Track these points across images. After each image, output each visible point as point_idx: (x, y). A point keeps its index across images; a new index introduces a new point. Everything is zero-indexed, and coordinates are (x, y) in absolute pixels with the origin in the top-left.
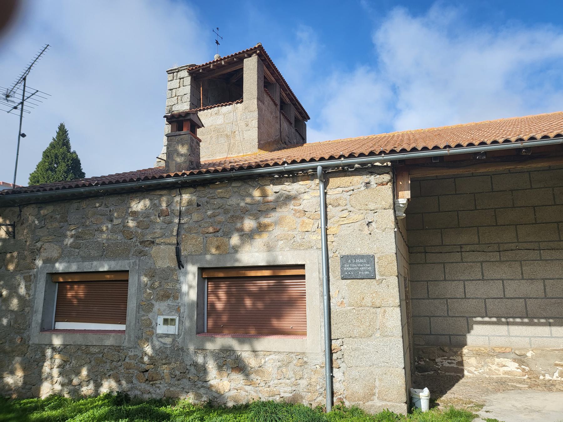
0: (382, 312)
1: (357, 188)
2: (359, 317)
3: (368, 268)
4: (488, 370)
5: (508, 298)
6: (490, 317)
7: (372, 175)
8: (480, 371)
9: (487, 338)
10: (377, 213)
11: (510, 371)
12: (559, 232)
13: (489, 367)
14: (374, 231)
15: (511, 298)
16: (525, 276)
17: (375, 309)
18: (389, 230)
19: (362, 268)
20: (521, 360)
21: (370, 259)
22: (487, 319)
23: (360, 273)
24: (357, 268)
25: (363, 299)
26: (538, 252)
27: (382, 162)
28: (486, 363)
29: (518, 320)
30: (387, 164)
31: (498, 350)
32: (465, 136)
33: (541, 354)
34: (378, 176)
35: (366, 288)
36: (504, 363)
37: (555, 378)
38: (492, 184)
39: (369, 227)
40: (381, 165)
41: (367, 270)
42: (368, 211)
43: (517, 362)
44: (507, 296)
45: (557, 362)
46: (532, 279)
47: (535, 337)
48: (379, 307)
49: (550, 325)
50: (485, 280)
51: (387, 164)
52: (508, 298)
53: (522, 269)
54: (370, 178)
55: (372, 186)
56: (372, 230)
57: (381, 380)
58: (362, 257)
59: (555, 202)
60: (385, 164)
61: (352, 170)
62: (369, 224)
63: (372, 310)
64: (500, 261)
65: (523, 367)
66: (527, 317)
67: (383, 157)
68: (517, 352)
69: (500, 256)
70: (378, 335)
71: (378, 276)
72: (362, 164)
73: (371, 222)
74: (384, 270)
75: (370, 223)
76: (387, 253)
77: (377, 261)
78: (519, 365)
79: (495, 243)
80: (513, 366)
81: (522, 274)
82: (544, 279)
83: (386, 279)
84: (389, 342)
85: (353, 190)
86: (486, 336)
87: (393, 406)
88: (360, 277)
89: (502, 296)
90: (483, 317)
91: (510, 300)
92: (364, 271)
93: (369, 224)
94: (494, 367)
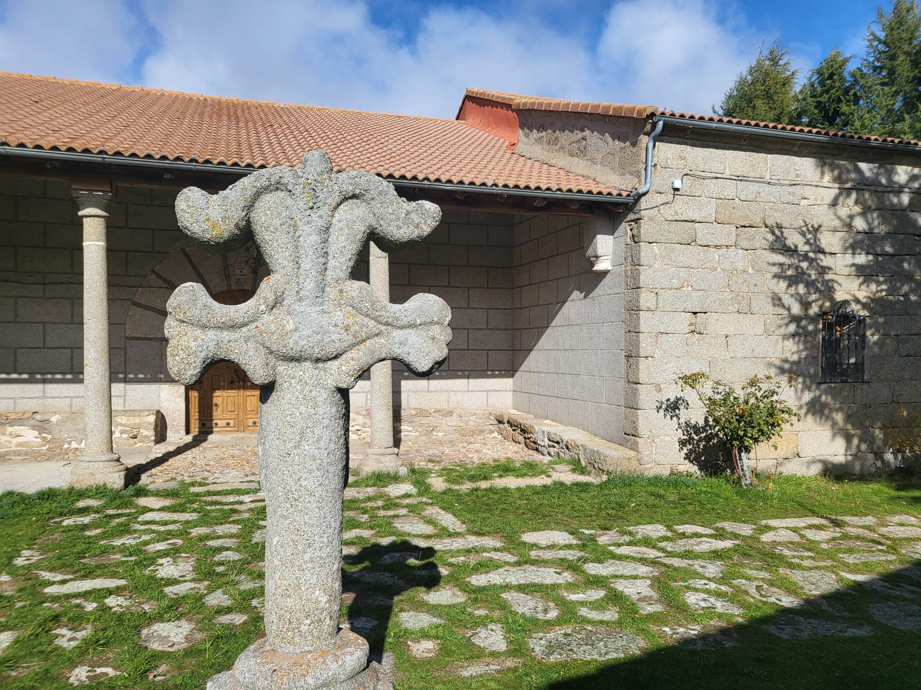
5: (49, 348)
6: (20, 374)
12: (126, 265)
15: (54, 348)
20: (42, 426)
22: (14, 376)
29: (59, 376)
32: (335, 156)
33: (68, 418)
36: (18, 433)
44: (48, 345)
50: (18, 322)
52: (49, 348)
65: (44, 435)
69: (44, 290)
78: (40, 434)
79: (39, 272)
81: (72, 316)
86: (12, 398)
89: (40, 346)
90: (8, 373)
91: (50, 350)
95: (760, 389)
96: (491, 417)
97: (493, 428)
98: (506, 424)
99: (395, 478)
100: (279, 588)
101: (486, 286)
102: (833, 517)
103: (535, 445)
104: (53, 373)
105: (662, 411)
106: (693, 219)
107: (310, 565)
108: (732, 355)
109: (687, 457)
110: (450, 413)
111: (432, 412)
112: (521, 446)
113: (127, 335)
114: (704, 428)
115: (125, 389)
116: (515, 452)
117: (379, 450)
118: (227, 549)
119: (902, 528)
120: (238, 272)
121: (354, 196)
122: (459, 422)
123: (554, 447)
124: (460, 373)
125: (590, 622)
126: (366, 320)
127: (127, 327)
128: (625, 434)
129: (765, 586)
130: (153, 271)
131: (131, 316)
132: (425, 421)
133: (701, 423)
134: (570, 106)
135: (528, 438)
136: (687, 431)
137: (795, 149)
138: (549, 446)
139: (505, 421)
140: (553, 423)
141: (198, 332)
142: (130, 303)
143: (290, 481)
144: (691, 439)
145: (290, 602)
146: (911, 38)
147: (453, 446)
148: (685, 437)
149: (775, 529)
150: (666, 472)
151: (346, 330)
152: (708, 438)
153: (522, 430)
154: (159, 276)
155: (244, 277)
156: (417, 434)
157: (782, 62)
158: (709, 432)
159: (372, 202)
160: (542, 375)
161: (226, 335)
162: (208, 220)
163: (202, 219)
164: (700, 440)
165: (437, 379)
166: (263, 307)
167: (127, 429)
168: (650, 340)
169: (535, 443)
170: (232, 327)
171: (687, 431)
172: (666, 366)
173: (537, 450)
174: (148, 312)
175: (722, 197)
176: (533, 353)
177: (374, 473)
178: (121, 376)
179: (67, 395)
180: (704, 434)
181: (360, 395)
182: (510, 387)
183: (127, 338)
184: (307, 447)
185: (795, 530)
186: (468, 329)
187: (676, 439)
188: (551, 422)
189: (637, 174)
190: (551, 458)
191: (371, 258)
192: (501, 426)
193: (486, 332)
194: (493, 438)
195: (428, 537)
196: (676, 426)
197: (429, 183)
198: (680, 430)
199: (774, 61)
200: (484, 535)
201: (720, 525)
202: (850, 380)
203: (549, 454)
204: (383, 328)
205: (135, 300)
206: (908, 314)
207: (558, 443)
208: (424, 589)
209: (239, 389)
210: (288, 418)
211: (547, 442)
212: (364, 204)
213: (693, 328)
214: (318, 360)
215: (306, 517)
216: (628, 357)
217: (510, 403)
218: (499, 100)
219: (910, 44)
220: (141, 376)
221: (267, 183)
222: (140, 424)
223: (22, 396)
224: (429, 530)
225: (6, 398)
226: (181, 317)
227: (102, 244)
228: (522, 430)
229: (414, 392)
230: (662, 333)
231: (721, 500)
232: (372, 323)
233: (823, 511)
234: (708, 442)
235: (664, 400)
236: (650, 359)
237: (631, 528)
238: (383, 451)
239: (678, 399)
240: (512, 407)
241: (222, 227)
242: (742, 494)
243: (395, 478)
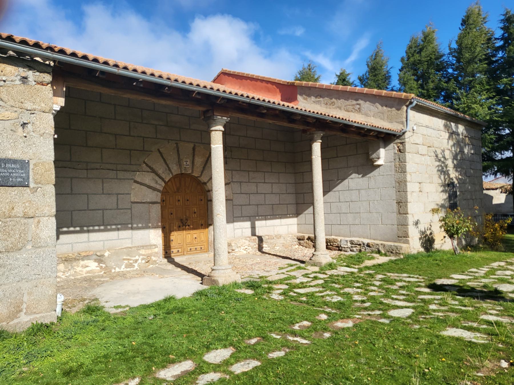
0: (36, 222)
1: (10, 80)
2: (7, 230)
3: (22, 175)
4: (74, 273)
5: (90, 210)
6: (75, 227)
7: (30, 70)
8: (67, 275)
9: (71, 245)
10: (35, 115)
11: (91, 270)
13: (75, 270)
14: (31, 134)
16: (105, 192)
17: (27, 219)
18: (48, 136)
19: (14, 174)
20: (100, 259)
21: (24, 165)
22: (72, 229)
23: (11, 179)
24: (7, 174)
25: (13, 209)
26: (115, 172)
27: (45, 58)
28: (72, 267)
29: (96, 228)
30: (50, 63)
31: (83, 254)
34: (38, 74)
35: (17, 197)
36: (87, 265)
37: (122, 270)
38: (85, 108)
39: (25, 129)
40: (42, 61)
41: (21, 177)
42: (23, 110)
43: (97, 262)
44: (90, 208)
45: (125, 257)
46: (109, 194)
47: (107, 240)
48: (32, 218)
49: (118, 229)
50: (74, 194)
51: (50, 63)
53: (103, 186)
54: (28, 73)
55: (30, 83)
56: (28, 133)
57: (30, 294)
58: (15, 161)
59: (156, 136)
60: (47, 62)
61: (4, 56)
62: (24, 125)
63: (23, 221)
64: (88, 178)
65: (101, 265)
66: (103, 225)
67: (48, 54)
68: (98, 254)
69: (87, 174)
70: (29, 247)
71: (32, 184)
72: (20, 53)
73: (27, 124)
74: (41, 178)
75: (25, 124)
76: (44, 160)
77: (32, 168)
78: (99, 264)
80: (93, 265)
81: (103, 189)
82: (118, 194)
83: (41, 188)
84: (42, 253)
85: (4, 81)
86: (70, 243)
87: (43, 317)
88: (11, 184)
90: (68, 227)
91: (91, 211)
92: (16, 177)
93: (24, 125)
94: (78, 269)
101: (270, 171)
104: (93, 226)
113: (132, 201)
115: (132, 234)
120: (185, 163)
124: (278, 216)
127: (132, 196)
128: (398, 237)
130: (144, 162)
131: (134, 189)
132: (272, 241)
137: (439, 116)
142: (133, 181)
154: (147, 165)
155: (188, 166)
156: (269, 248)
167: (145, 257)
174: (142, 187)
178: (130, 226)
179: (101, 239)
182: (296, 223)
183: (133, 203)
189: (402, 123)
205: (136, 179)
209: (183, 230)
211: (349, 245)
216: (398, 203)
220: (140, 225)
222: (151, 253)
223: (76, 242)
225: (67, 244)
227: (213, 146)
229: (261, 227)
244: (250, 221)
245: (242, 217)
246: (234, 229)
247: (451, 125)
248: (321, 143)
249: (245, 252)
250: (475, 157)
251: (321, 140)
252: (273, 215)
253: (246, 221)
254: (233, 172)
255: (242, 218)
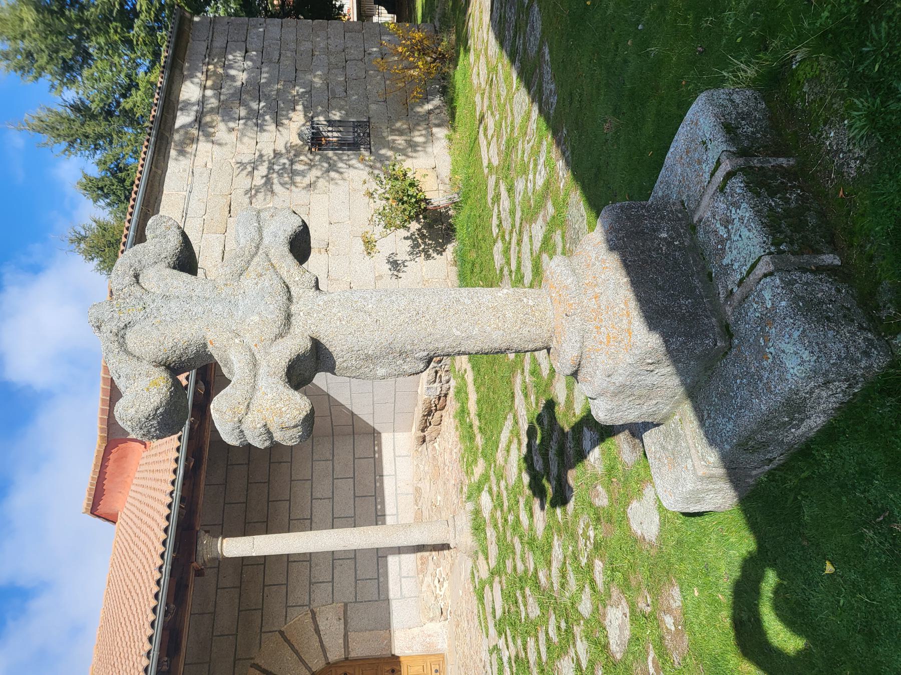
95: (376, 190)
96: (420, 450)
97: (430, 448)
98: (426, 433)
99: (477, 512)
100: (498, 325)
101: (289, 464)
102: (478, 122)
103: (442, 398)
105: (400, 275)
106: (221, 252)
107: (475, 299)
108: (347, 219)
109: (440, 253)
110: (418, 490)
111: (417, 508)
112: (444, 414)
114: (414, 241)
116: (448, 419)
117: (450, 533)
118: (547, 633)
119: (481, 73)
121: (137, 276)
122: (426, 481)
123: (440, 376)
124: (378, 484)
125: (564, 246)
126: (253, 263)
129: (527, 138)
133: (409, 242)
134: (106, 387)
135: (436, 406)
136: (417, 254)
137: (160, 172)
138: (441, 382)
139: (422, 434)
140: (420, 384)
141: (259, 394)
143: (402, 318)
144: (423, 250)
145: (509, 315)
146: (68, 120)
147: (448, 480)
148: (423, 254)
149: (489, 160)
150: (455, 269)
151: (261, 276)
152: (423, 236)
153: (429, 415)
157: (83, 233)
158: (417, 236)
159: (143, 263)
160: (375, 399)
161: (262, 371)
162: (148, 389)
163: (146, 394)
164: (424, 243)
165: (384, 507)
166: (237, 341)
168: (334, 286)
169: (439, 398)
170: (255, 365)
171: (417, 254)
172: (359, 272)
173: (446, 395)
175: (201, 229)
176: (356, 412)
177: (474, 535)
180: (419, 240)
181: (404, 584)
182: (391, 434)
184: (370, 306)
185: (489, 144)
186: (333, 479)
187: (424, 262)
188: (420, 388)
190: (452, 379)
191: (254, 555)
192: (427, 439)
193: (336, 462)
194: (439, 446)
195: (520, 443)
196: (413, 262)
197: (175, 492)
198: (416, 260)
199: (81, 239)
200: (513, 393)
201: (490, 201)
202: (368, 131)
203: (448, 382)
204: (261, 251)
206: (311, 91)
207: (436, 372)
208: (556, 408)
210: (344, 323)
211: (437, 385)
212: (144, 271)
213: (323, 251)
214: (290, 299)
215: (433, 304)
217: (406, 434)
218: (98, 470)
219: (74, 121)
221: (116, 343)
224: (514, 446)
226: (243, 407)
228: (429, 415)
230: (328, 276)
231: (472, 214)
232: (256, 259)
233: (474, 133)
234: (426, 237)
235: (390, 273)
236: (352, 285)
237: (498, 272)
238: (451, 529)
239: (389, 262)
240: (409, 433)
241: (156, 376)
242: (467, 197)
243: (477, 512)
244: (386, 557)
245: (378, 579)
246: (403, 597)
247: (182, 127)
248: (224, 538)
249: (446, 585)
250: (254, 41)
251: (218, 538)
252: (375, 496)
253: (386, 566)
254: (290, 603)
255: (381, 579)
